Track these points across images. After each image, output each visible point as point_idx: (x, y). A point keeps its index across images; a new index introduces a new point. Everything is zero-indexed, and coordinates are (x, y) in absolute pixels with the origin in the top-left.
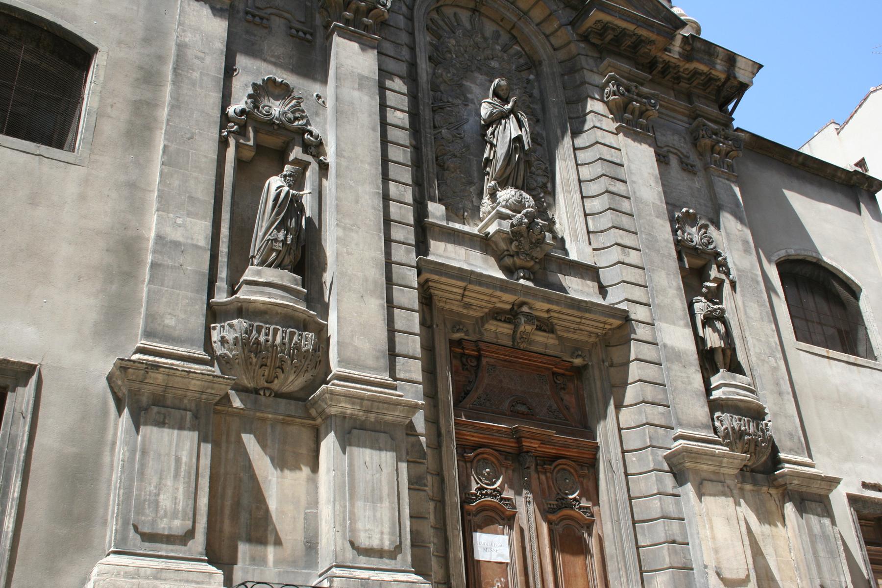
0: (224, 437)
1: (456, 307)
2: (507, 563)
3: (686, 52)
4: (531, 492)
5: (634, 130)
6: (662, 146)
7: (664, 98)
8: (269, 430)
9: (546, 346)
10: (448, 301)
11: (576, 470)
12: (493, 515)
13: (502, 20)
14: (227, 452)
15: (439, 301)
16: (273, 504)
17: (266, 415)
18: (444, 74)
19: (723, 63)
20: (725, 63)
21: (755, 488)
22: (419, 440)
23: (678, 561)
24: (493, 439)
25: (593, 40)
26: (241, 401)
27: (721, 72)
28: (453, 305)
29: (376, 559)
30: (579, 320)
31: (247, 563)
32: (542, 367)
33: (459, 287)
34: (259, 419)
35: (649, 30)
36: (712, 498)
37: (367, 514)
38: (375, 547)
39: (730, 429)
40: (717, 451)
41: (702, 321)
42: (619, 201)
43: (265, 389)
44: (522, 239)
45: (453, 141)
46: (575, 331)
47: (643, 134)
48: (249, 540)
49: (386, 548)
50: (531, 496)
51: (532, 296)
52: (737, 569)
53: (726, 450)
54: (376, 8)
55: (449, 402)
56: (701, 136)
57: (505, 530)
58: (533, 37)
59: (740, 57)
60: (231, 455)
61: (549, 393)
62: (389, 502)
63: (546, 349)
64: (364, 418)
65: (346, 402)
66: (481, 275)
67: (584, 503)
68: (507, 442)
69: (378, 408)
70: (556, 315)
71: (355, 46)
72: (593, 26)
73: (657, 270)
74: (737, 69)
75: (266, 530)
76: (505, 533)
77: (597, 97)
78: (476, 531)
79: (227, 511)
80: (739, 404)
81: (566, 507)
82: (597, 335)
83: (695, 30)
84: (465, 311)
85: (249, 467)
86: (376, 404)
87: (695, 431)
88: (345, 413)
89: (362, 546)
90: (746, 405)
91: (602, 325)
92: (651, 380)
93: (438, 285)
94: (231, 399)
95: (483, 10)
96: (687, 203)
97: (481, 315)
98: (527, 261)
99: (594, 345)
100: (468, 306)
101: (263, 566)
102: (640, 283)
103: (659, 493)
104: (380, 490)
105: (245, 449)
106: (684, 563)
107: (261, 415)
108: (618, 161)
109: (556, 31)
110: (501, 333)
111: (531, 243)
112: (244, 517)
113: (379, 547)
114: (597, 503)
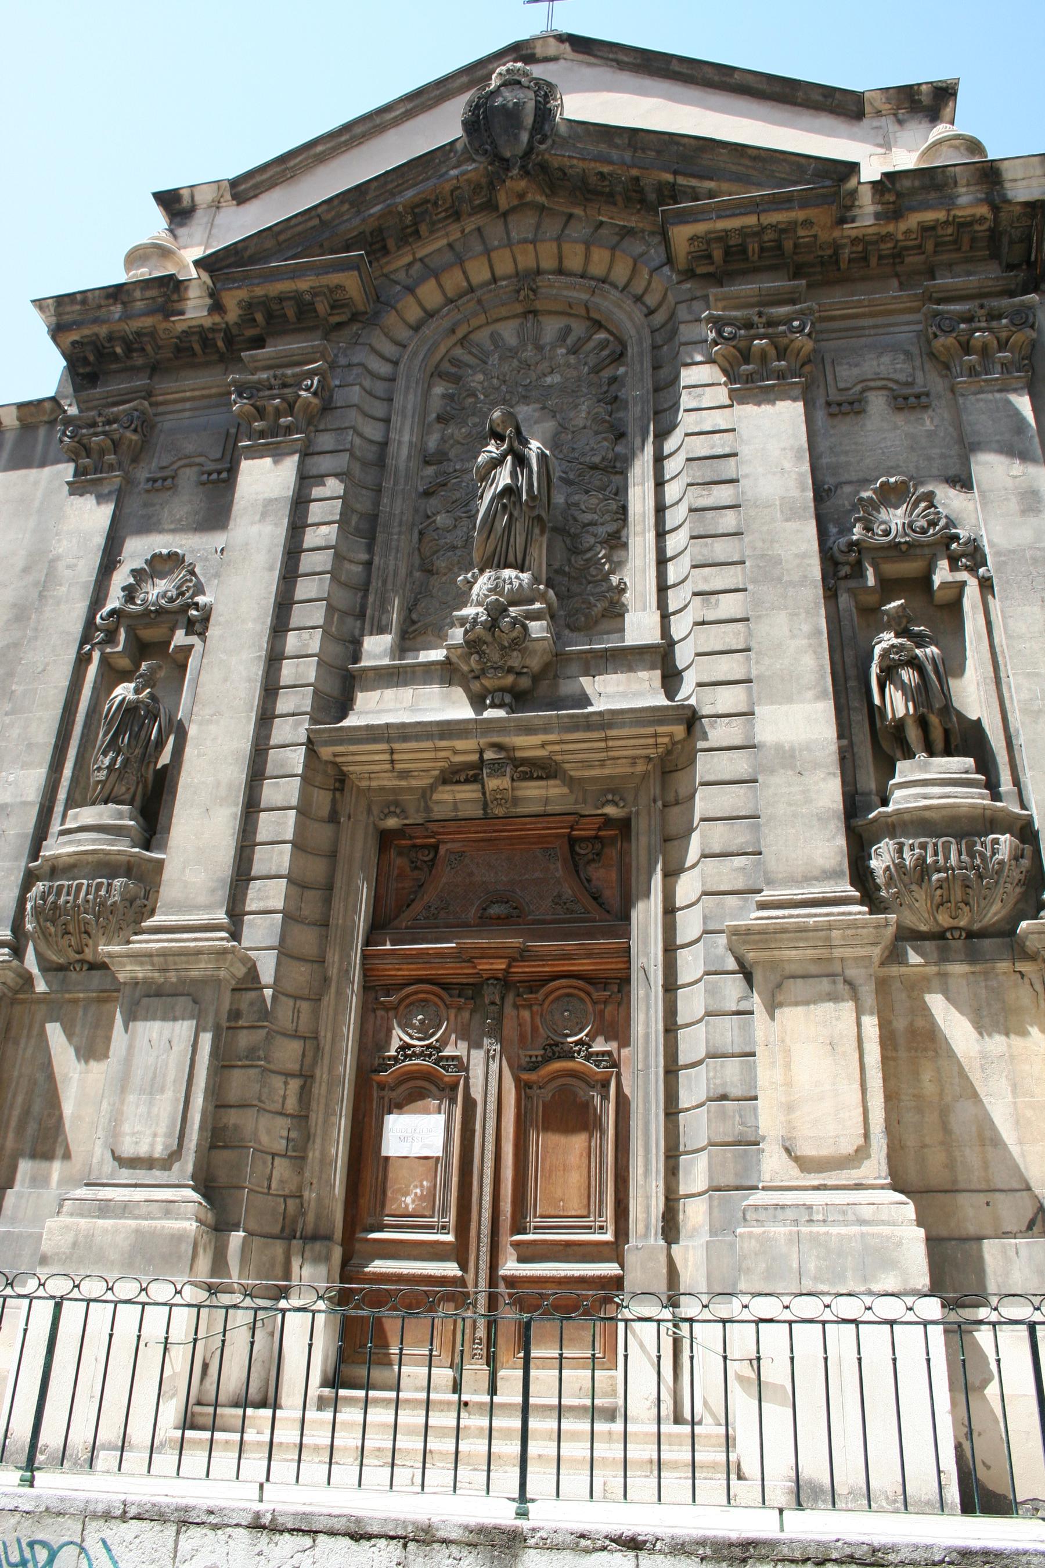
0: (25, 1032)
1: (388, 781)
2: (438, 1158)
3: (891, 206)
4: (500, 1040)
5: (760, 387)
6: (849, 385)
7: (859, 301)
8: (80, 1013)
9: (547, 801)
10: (372, 775)
11: (589, 994)
12: (426, 1084)
13: (570, 307)
14: (25, 1049)
15: (360, 779)
16: (68, 1109)
17: (77, 995)
18: (456, 432)
19: (972, 188)
20: (977, 188)
21: (978, 968)
22: (263, 996)
23: (728, 1131)
24: (431, 968)
25: (700, 270)
26: (47, 983)
27: (971, 205)
28: (383, 779)
29: (143, 1172)
30: (602, 745)
31: (26, 1185)
32: (550, 835)
33: (382, 752)
34: (70, 1001)
35: (782, 209)
36: (800, 1010)
37: (140, 1110)
38: (142, 1155)
39: (893, 869)
40: (811, 920)
41: (878, 677)
42: (713, 518)
43: (78, 961)
44: (484, 647)
45: (455, 526)
46: (602, 763)
47: (778, 385)
48: (33, 1156)
49: (157, 1155)
50: (498, 1047)
51: (498, 731)
52: (837, 1136)
53: (859, 913)
54: (299, 396)
55: (353, 927)
56: (931, 336)
57: (443, 1107)
58: (616, 310)
59: (1006, 162)
60: (29, 1051)
61: (559, 874)
62: (174, 1091)
63: (546, 805)
64: (162, 980)
65: (131, 964)
66: (403, 725)
67: (599, 1046)
68: (457, 968)
69: (175, 964)
70: (557, 748)
71: (268, 461)
72: (693, 249)
73: (767, 615)
74: (1007, 185)
75: (55, 1142)
76: (443, 1111)
77: (699, 358)
78: (390, 1113)
79: (13, 1123)
80: (927, 814)
81: (559, 1057)
82: (648, 759)
83: (962, 148)
84: (403, 783)
85: (47, 1066)
86: (170, 958)
87: (803, 888)
88: (136, 978)
89: (125, 1155)
90: (944, 812)
91: (651, 741)
92: (726, 815)
93: (350, 759)
94: (35, 983)
95: (538, 305)
96: (898, 466)
97: (431, 781)
98: (500, 678)
99: (645, 776)
100: (405, 774)
101: (42, 1188)
102: (734, 647)
103: (708, 1014)
104: (165, 1075)
105: (47, 1042)
106: (740, 1134)
107: (71, 996)
108: (727, 450)
109: (649, 283)
110: (464, 801)
111: (503, 648)
112: (32, 1128)
113: (147, 1155)
114: (625, 1041)
